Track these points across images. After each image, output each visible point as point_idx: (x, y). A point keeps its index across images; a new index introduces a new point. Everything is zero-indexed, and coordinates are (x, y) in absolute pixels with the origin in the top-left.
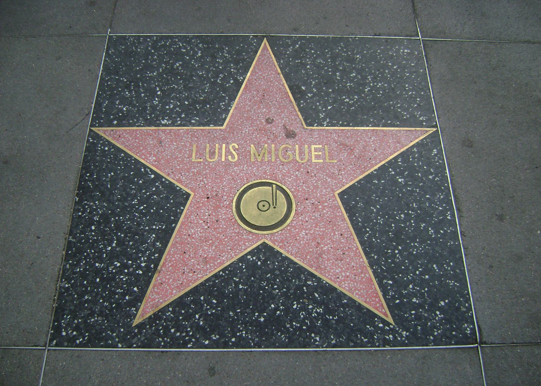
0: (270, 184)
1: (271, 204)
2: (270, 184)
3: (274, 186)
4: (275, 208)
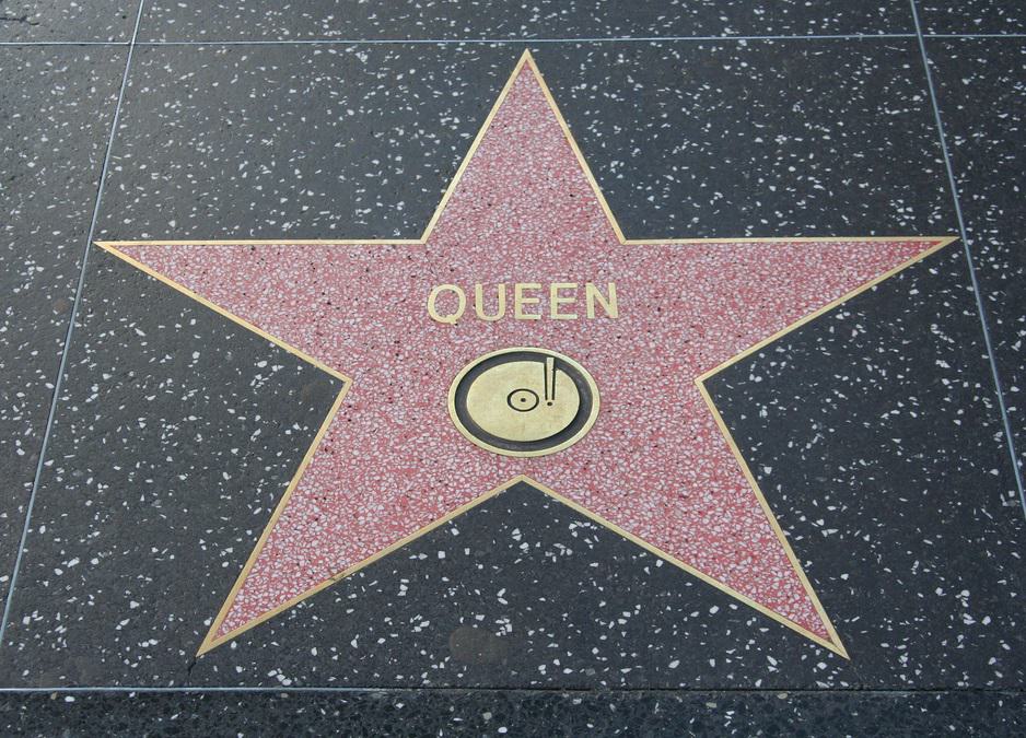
0: (541, 357)
1: (542, 395)
2: (541, 357)
3: (550, 362)
4: (549, 404)
